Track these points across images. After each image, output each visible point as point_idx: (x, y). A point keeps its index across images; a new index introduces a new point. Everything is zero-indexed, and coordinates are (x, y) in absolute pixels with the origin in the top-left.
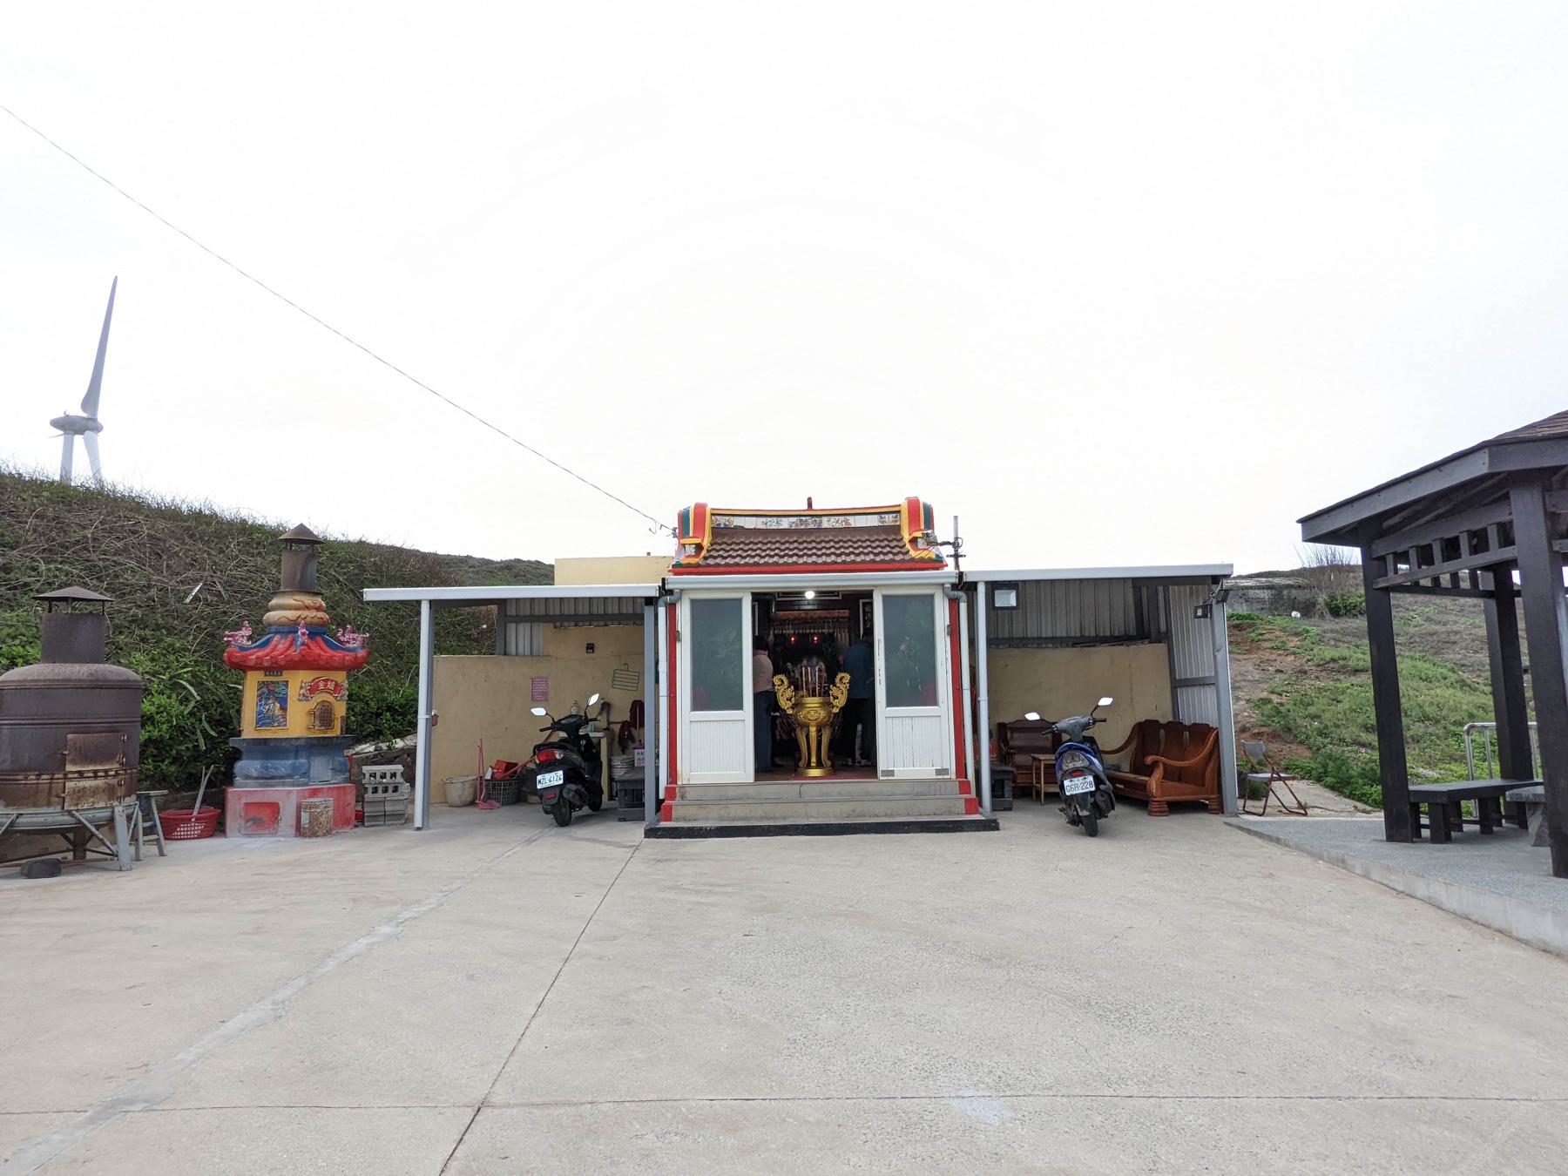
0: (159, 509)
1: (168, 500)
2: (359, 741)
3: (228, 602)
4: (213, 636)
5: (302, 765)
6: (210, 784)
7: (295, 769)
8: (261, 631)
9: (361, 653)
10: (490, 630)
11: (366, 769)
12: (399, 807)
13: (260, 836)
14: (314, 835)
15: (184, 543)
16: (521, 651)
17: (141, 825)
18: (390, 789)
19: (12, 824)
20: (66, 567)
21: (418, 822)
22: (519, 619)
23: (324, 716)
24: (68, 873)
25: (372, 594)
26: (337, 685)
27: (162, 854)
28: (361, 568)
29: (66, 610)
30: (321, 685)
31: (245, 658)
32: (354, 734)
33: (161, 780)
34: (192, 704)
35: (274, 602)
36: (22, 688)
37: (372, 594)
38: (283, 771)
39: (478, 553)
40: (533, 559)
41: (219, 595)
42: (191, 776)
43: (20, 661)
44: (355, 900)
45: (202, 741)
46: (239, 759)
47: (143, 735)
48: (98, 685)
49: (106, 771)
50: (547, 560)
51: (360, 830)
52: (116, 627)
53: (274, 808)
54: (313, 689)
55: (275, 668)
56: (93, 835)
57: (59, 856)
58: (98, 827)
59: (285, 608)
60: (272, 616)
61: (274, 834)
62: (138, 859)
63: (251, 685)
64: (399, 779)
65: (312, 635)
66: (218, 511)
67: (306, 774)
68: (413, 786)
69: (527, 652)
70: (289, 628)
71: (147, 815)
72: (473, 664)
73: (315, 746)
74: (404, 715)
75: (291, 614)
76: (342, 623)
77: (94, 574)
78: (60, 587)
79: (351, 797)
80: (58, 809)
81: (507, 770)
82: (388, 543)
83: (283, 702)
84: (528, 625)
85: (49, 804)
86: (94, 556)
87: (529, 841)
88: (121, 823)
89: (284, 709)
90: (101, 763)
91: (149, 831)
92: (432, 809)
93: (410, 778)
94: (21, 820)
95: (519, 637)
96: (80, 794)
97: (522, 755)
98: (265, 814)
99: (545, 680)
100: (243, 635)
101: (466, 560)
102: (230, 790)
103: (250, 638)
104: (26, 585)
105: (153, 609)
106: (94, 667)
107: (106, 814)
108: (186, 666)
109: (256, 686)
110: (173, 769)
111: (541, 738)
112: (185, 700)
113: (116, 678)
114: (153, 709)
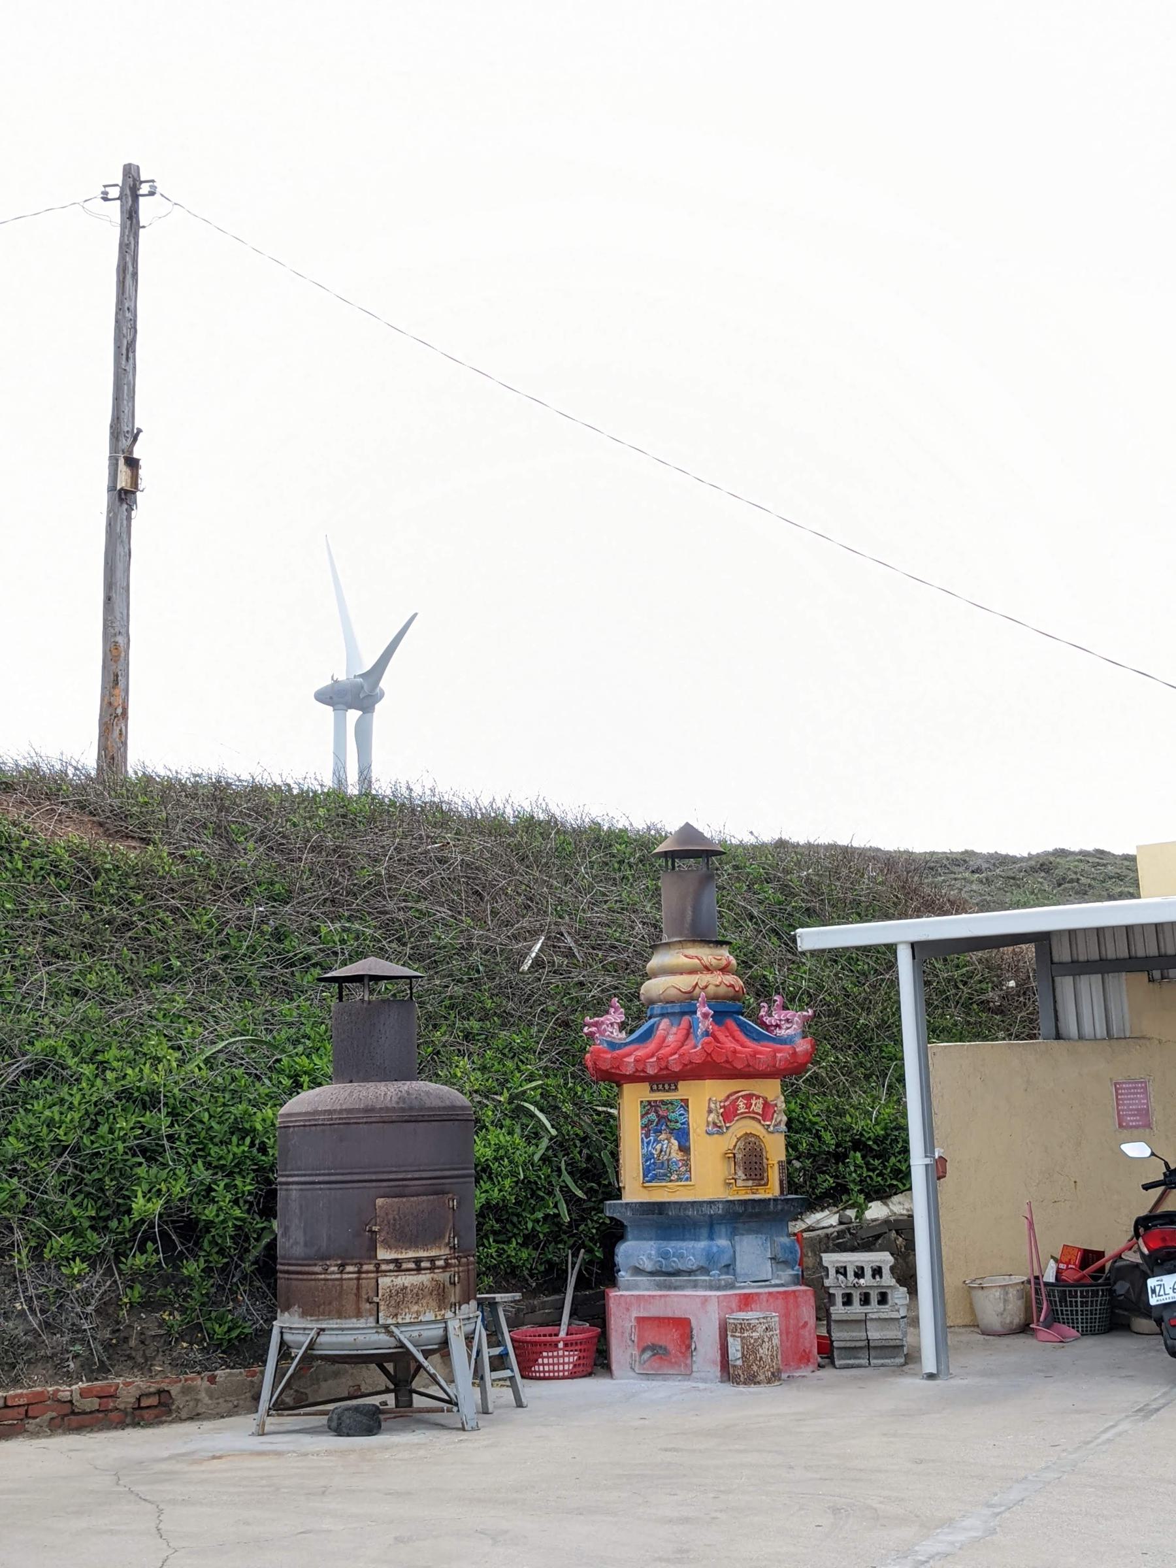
0: (473, 818)
1: (485, 802)
2: (814, 1204)
3: (586, 965)
4: (566, 1024)
5: (721, 1251)
6: (581, 1283)
7: (711, 1258)
8: (638, 1013)
9: (803, 1046)
10: (1023, 990)
11: (831, 1259)
12: (891, 1334)
13: (665, 1376)
14: (752, 1380)
15: (512, 872)
16: (1088, 1030)
17: (487, 1353)
18: (874, 1298)
19: (311, 1346)
20: (356, 926)
21: (929, 1363)
22: (1078, 968)
23: (751, 1162)
24: (390, 1430)
25: (811, 938)
26: (766, 1104)
27: (519, 1404)
28: (785, 888)
29: (360, 994)
30: (741, 1104)
31: (619, 1061)
32: (805, 1192)
33: (507, 1275)
34: (545, 1143)
35: (656, 961)
36: (312, 1124)
37: (811, 938)
38: (692, 1262)
39: (985, 844)
40: (1090, 847)
41: (569, 954)
42: (554, 1264)
43: (305, 1079)
44: (836, 1510)
45: (563, 1207)
46: (621, 1237)
47: (480, 1199)
48: (412, 1116)
49: (432, 1260)
50: (1118, 847)
51: (828, 1373)
52: (429, 1017)
53: (683, 1326)
54: (729, 1114)
55: (665, 1079)
56: (420, 1366)
57: (376, 1400)
58: (427, 1354)
59: (680, 971)
60: (653, 987)
61: (688, 1375)
62: (485, 1411)
63: (631, 1106)
64: (888, 1279)
65: (719, 1016)
66: (558, 814)
67: (729, 1268)
68: (913, 1291)
69: (1101, 1031)
70: (683, 1006)
71: (494, 1337)
72: (996, 1056)
73: (744, 1216)
74: (883, 1156)
75: (684, 982)
76: (763, 990)
77: (393, 936)
78: (351, 959)
79: (808, 1313)
80: (371, 1322)
81: (1084, 1264)
82: (824, 839)
83: (682, 1135)
84: (1096, 979)
85: (358, 1315)
86: (391, 905)
87: (1146, 1412)
88: (458, 1347)
89: (685, 1149)
90: (425, 1247)
91: (499, 1363)
92: (951, 1340)
93: (907, 1278)
94: (323, 1339)
95: (1082, 1001)
96: (400, 1298)
97: (1113, 1237)
98: (668, 1339)
99: (1141, 1086)
100: (610, 1026)
101: (962, 860)
102: (613, 1294)
103: (622, 1026)
104: (307, 958)
105: (477, 984)
106: (406, 1086)
107: (436, 1332)
108: (530, 1079)
109: (638, 1111)
110: (524, 1255)
111: (1144, 1203)
112: (534, 1137)
113: (437, 1103)
114: (489, 1152)
